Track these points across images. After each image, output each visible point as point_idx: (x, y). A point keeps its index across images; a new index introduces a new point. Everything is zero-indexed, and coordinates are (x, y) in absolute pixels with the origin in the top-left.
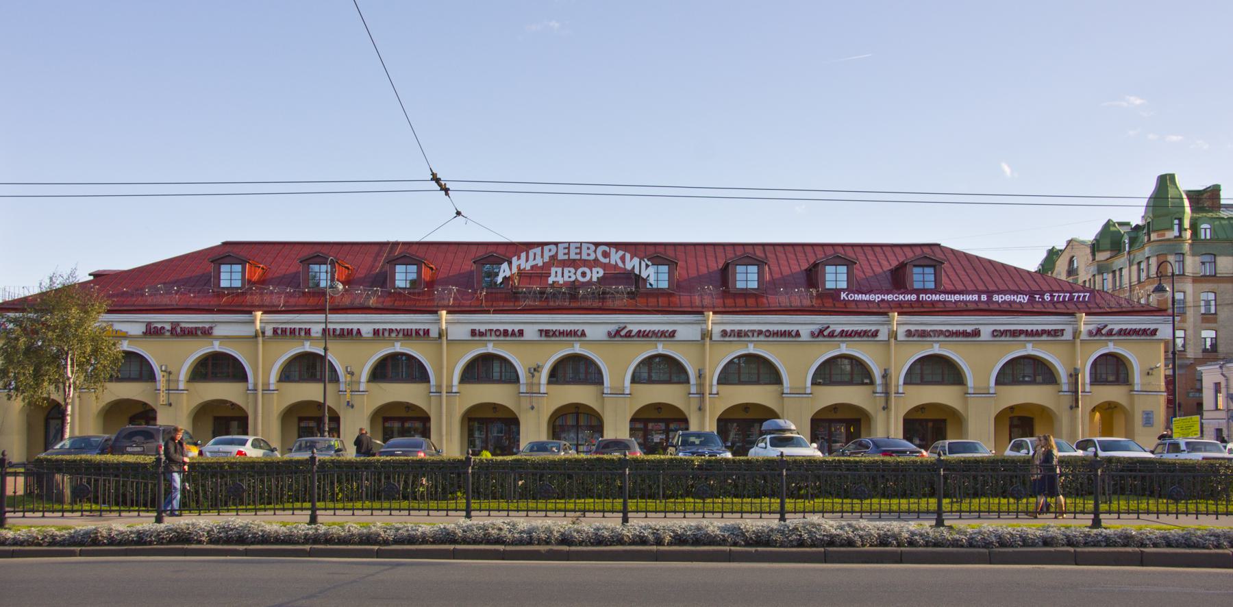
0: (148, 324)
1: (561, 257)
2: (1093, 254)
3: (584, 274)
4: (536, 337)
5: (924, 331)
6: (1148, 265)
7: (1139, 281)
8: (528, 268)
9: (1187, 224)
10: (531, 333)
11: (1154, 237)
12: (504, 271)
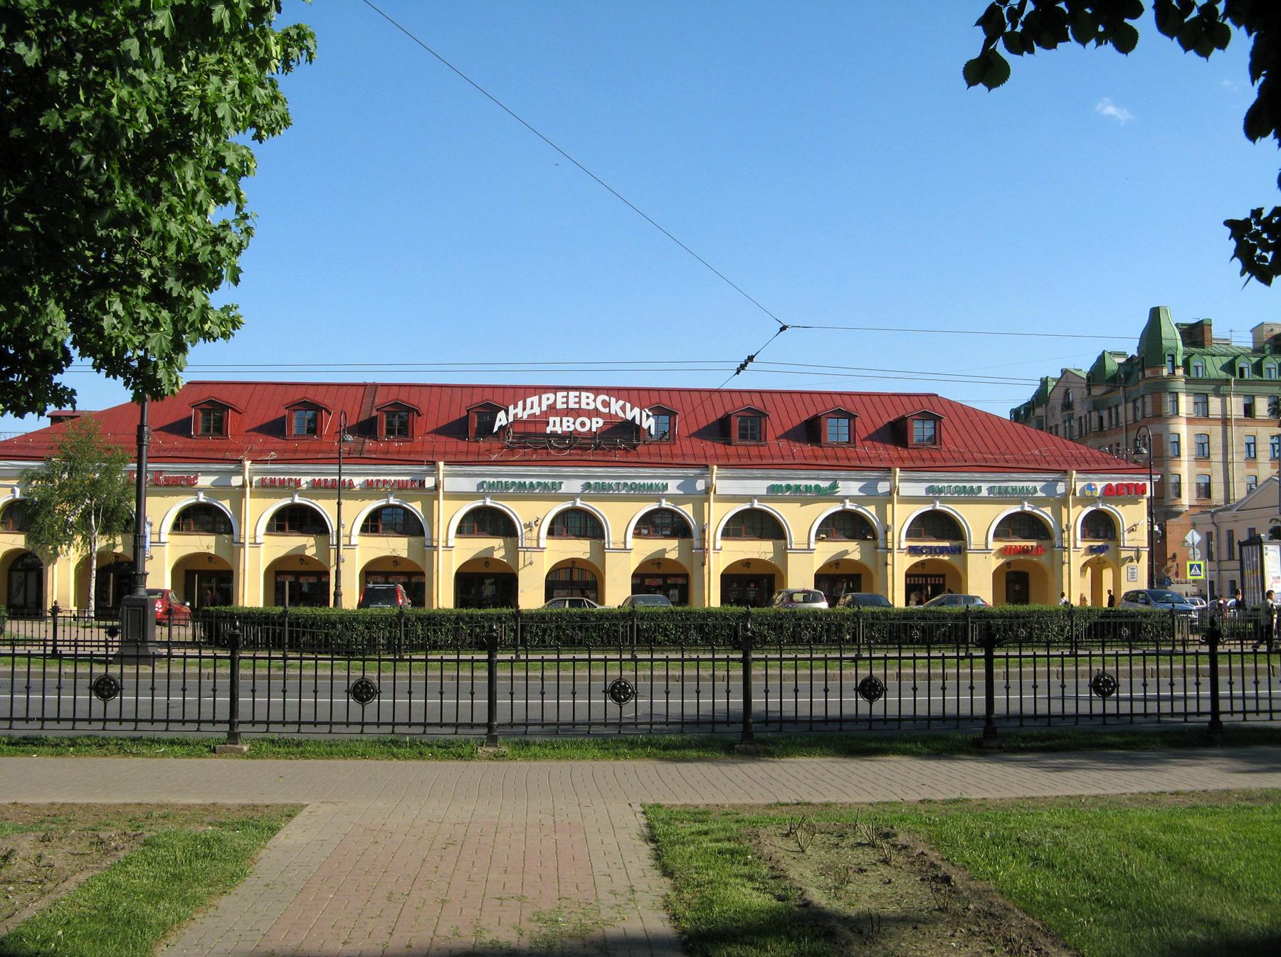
1: (559, 406)
2: (1089, 390)
3: (583, 424)
6: (1144, 403)
7: (1135, 421)
8: (525, 417)
9: (1179, 362)
11: (1148, 373)
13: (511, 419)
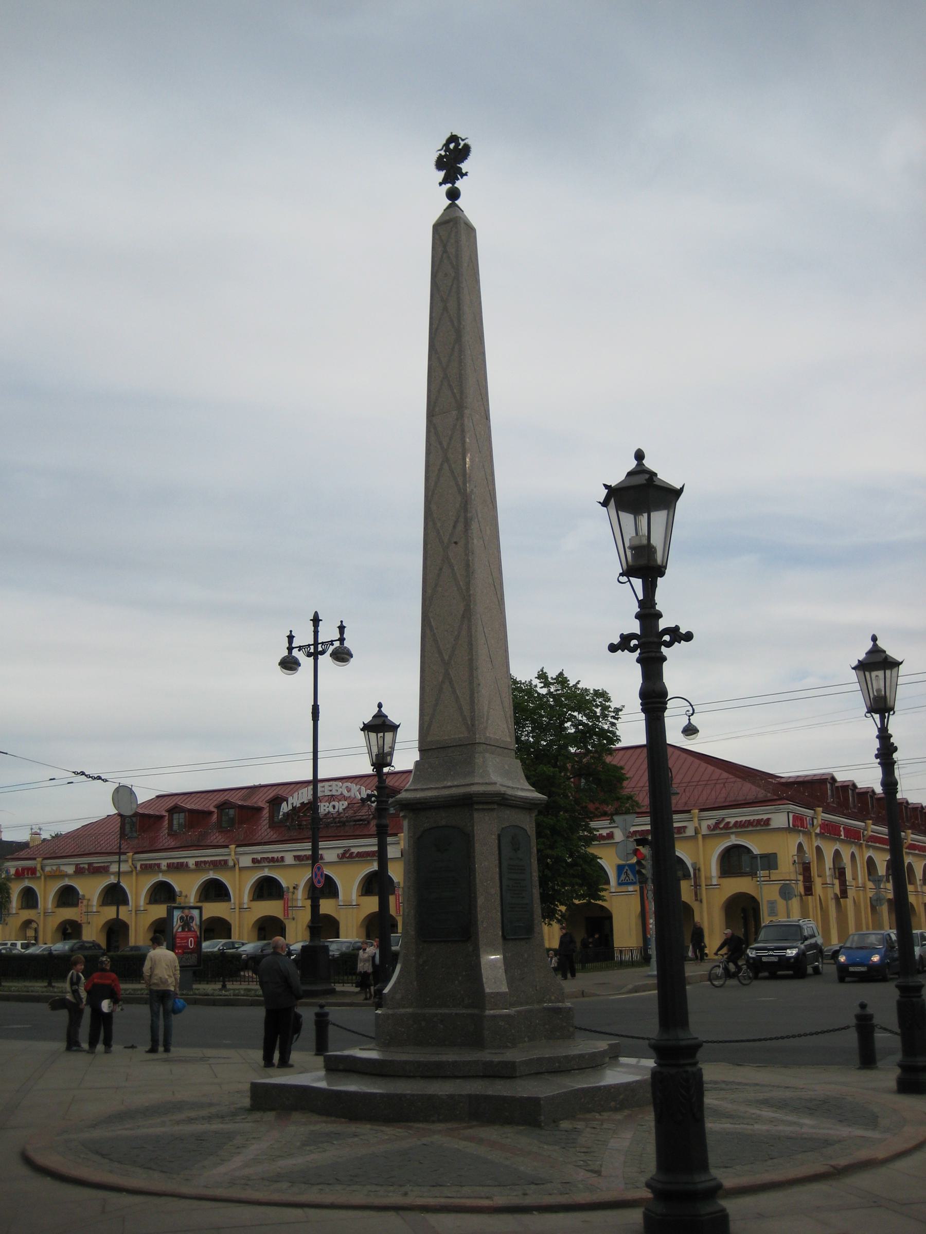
0: (77, 865)
4: (249, 864)
5: (273, 858)
10: (289, 859)
12: (285, 808)
13: (290, 807)
